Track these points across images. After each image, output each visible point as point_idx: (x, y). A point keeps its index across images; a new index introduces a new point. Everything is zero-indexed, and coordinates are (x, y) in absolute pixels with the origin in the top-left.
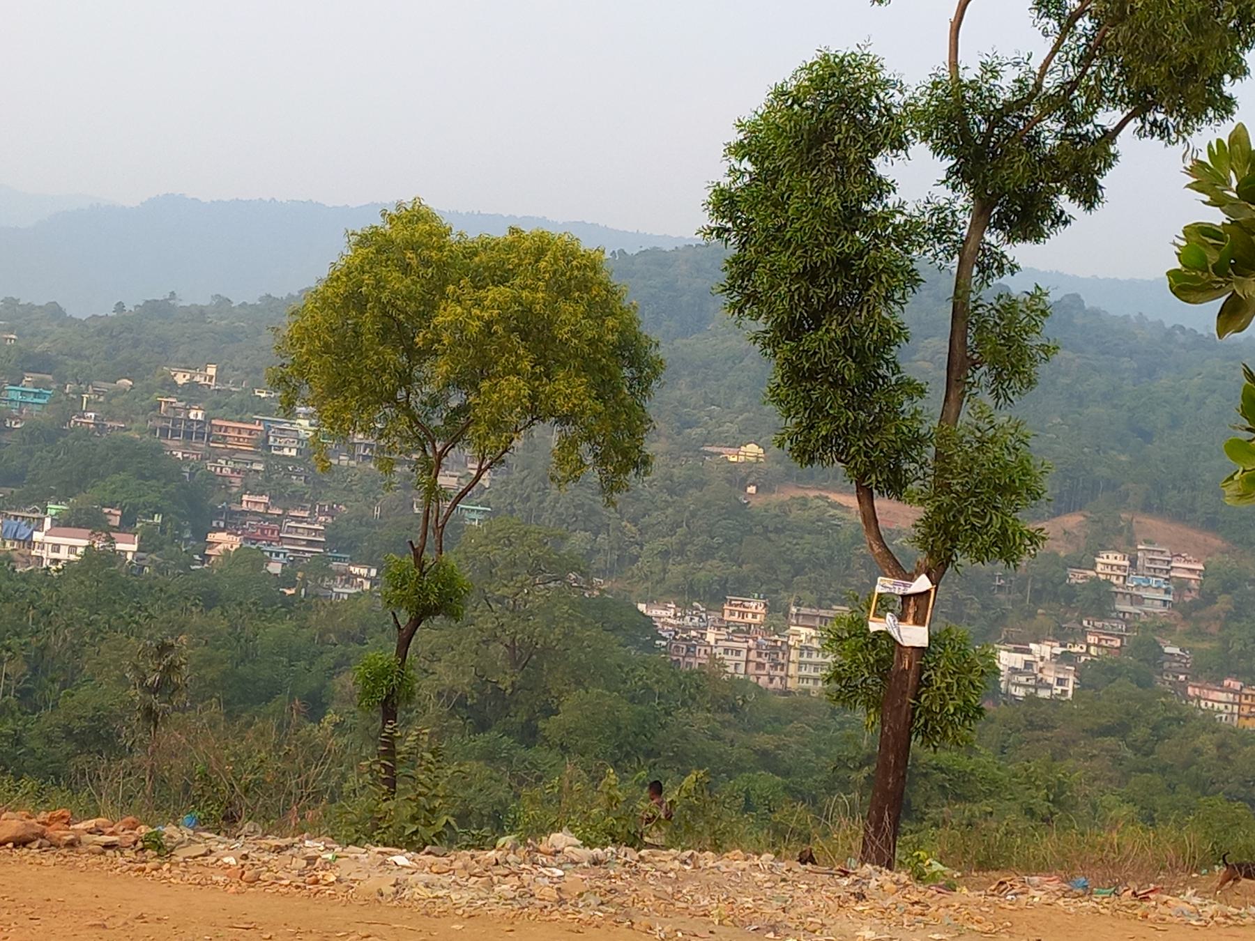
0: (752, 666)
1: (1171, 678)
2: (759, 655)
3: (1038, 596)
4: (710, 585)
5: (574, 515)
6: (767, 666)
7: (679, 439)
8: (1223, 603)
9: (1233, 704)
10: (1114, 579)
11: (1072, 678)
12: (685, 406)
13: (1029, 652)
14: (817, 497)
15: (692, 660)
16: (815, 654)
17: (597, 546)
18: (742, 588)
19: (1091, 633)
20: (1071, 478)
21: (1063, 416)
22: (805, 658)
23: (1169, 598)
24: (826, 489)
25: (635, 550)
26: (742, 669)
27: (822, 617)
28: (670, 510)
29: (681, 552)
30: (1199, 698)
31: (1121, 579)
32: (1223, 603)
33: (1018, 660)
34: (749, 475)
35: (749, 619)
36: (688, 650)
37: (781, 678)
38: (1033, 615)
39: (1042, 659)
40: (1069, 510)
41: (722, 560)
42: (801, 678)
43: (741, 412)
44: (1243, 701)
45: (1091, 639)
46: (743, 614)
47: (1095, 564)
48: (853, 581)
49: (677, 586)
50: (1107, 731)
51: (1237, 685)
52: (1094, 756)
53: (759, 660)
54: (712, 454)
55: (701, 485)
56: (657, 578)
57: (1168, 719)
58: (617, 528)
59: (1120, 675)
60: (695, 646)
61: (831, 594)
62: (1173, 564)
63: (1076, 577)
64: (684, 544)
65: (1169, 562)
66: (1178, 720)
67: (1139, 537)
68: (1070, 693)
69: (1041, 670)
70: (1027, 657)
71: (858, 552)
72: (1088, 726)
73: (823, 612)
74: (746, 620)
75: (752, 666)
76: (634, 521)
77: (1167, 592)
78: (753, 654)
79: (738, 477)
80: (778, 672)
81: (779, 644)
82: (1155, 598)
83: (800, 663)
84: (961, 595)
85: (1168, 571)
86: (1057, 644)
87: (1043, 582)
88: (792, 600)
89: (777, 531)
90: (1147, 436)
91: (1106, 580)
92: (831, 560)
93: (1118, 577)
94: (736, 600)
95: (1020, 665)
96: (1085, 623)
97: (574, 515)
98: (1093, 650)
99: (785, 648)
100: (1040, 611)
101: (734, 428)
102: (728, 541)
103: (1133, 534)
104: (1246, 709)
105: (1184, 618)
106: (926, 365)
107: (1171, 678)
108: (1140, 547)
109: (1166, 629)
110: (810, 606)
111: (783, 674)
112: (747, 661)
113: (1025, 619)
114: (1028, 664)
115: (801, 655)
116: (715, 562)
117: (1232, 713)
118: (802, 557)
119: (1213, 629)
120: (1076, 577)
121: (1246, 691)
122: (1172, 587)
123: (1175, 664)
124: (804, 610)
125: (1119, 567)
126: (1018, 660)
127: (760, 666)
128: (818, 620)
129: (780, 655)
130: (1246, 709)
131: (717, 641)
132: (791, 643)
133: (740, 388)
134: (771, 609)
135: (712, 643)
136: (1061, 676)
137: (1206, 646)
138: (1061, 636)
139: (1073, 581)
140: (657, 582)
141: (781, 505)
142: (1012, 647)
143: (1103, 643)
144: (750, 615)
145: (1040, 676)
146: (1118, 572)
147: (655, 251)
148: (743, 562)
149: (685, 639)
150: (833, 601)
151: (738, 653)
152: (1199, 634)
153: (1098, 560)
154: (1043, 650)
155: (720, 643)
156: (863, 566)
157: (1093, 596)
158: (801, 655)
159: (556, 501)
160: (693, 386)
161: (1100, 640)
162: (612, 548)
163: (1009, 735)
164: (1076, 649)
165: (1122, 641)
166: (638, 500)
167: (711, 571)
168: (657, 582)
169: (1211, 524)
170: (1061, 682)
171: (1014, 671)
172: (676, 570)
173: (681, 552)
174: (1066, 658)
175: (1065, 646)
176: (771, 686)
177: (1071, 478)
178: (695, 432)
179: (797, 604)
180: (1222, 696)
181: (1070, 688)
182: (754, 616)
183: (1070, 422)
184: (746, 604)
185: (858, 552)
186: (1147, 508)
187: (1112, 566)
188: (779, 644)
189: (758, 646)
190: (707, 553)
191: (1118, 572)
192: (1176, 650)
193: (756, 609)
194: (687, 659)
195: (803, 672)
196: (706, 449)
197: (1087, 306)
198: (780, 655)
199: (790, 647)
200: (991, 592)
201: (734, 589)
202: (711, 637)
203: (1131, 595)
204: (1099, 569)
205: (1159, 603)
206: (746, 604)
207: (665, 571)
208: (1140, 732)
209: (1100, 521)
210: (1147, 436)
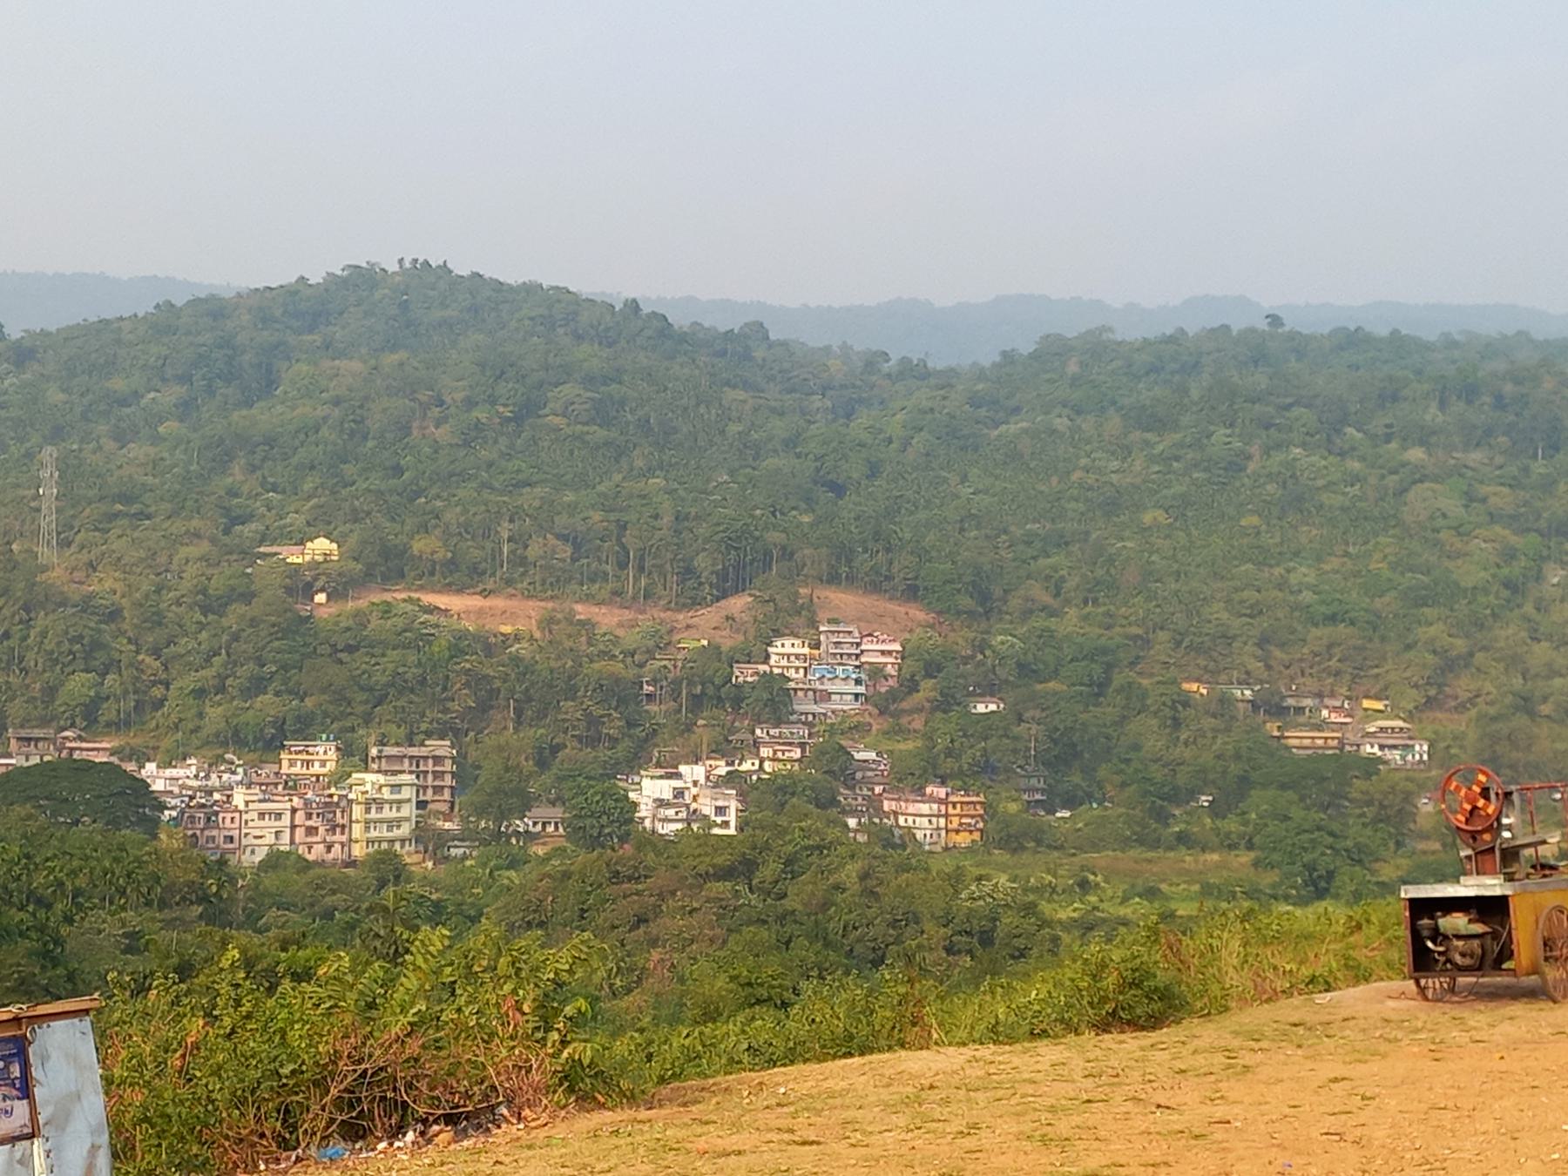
0: (300, 832)
1: (865, 792)
2: (309, 816)
3: (697, 703)
4: (262, 730)
5: (70, 652)
6: (321, 830)
7: (226, 539)
8: (928, 689)
9: (938, 816)
10: (792, 673)
11: (734, 805)
12: (236, 495)
13: (678, 776)
14: (404, 601)
15: (215, 833)
16: (387, 806)
17: (105, 691)
18: (306, 729)
19: (766, 744)
20: (736, 549)
21: (732, 473)
22: (373, 815)
23: (861, 689)
24: (421, 588)
25: (157, 692)
26: (286, 838)
27: (411, 757)
28: (204, 635)
29: (221, 689)
30: (896, 813)
31: (802, 671)
32: (928, 689)
33: (665, 789)
34: (316, 579)
35: (316, 769)
36: (209, 819)
37: (343, 845)
38: (689, 728)
39: (695, 783)
40: (737, 590)
41: (277, 694)
42: (370, 842)
43: (309, 498)
44: (951, 811)
45: (765, 752)
46: (308, 763)
47: (768, 657)
48: (454, 706)
49: (217, 735)
50: (726, 874)
51: (941, 792)
52: (694, 910)
53: (309, 823)
54: (264, 556)
55: (248, 597)
56: (191, 726)
57: (806, 848)
58: (131, 665)
59: (793, 794)
60: (216, 814)
61: (424, 727)
62: (863, 647)
63: (745, 674)
64: (222, 678)
65: (858, 644)
66: (820, 848)
67: (822, 615)
68: (733, 824)
69: (695, 798)
70: (678, 784)
71: (457, 668)
72: (702, 869)
73: (414, 751)
74: (312, 771)
75: (300, 832)
76: (156, 652)
77: (858, 682)
78: (300, 817)
79: (301, 584)
80: (338, 837)
81: (336, 799)
82: (844, 694)
83: (367, 822)
84: (598, 711)
85: (857, 656)
86: (722, 763)
87: (703, 684)
88: (373, 739)
89: (351, 649)
90: (838, 490)
91: (782, 675)
92: (423, 682)
93: (797, 669)
94: (296, 745)
95: (667, 795)
96: (758, 732)
97: (70, 652)
98: (768, 766)
99: (343, 803)
100: (701, 722)
101: (300, 520)
102: (285, 667)
103: (814, 613)
104: (956, 820)
105: (881, 713)
106: (557, 420)
107: (865, 792)
108: (822, 628)
109: (860, 729)
110: (397, 744)
111: (344, 838)
112: (293, 827)
113: (682, 734)
114: (679, 793)
115: (368, 811)
116: (268, 697)
117: (938, 828)
118: (384, 679)
119: (918, 723)
120: (745, 674)
121: (953, 799)
122: (863, 676)
123: (870, 774)
124: (389, 751)
125: (797, 656)
126: (665, 789)
127: (311, 831)
128: (406, 761)
129: (339, 814)
130: (956, 820)
131: (247, 803)
132: (352, 796)
133: (312, 468)
134: (345, 752)
135: (242, 807)
136: (720, 803)
137: (910, 745)
138: (724, 749)
139: (741, 679)
140: (192, 732)
141: (357, 614)
142: (661, 772)
143: (780, 754)
144: (317, 764)
145: (694, 806)
146: (797, 664)
147: (212, 298)
148: (305, 694)
149: (203, 806)
150: (429, 734)
151: (279, 816)
152: (898, 732)
153: (770, 649)
154: (693, 772)
155: (251, 806)
156: (467, 685)
157: (765, 696)
158: (368, 811)
159: (44, 634)
160: (253, 468)
161: (775, 752)
162: (126, 692)
163: (589, 893)
164: (746, 766)
165: (803, 751)
166: (160, 624)
167: (267, 704)
168: (192, 732)
169: (912, 593)
170: (720, 810)
171: (661, 803)
172: (215, 714)
173: (221, 689)
174: (731, 778)
175: (732, 764)
176: (331, 856)
177: (736, 549)
178: (249, 530)
179: (382, 743)
180: (925, 808)
181: (732, 817)
182: (323, 763)
183: (741, 479)
184: (311, 749)
185: (457, 668)
186: (833, 579)
187: (789, 656)
188: (336, 799)
189: (307, 803)
190: (257, 686)
191: (797, 664)
192: (872, 755)
193: (325, 756)
194: (206, 833)
195: (373, 834)
196: (262, 549)
197: (772, 336)
198: (339, 814)
199: (350, 802)
200: (638, 703)
201: (294, 732)
202: (239, 799)
203: (815, 691)
204: (772, 662)
205: (850, 697)
206: (311, 749)
207: (201, 715)
208: (768, 871)
209: (772, 600)
210: (838, 490)
